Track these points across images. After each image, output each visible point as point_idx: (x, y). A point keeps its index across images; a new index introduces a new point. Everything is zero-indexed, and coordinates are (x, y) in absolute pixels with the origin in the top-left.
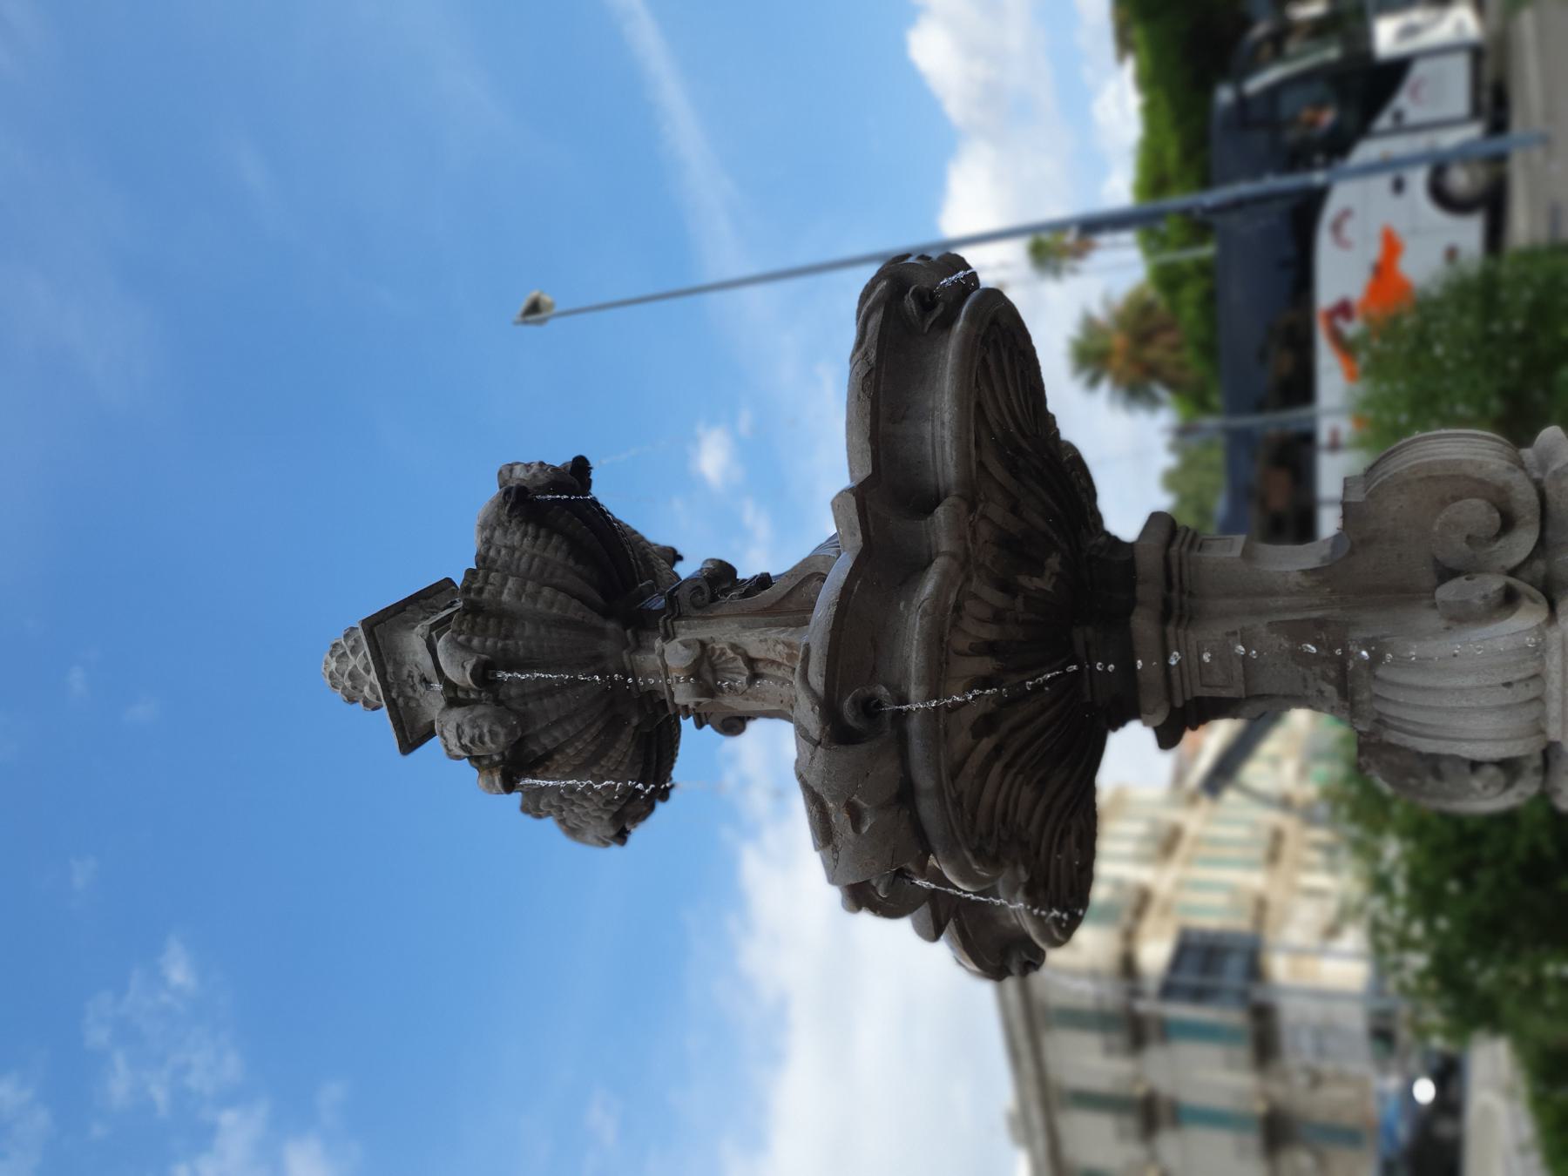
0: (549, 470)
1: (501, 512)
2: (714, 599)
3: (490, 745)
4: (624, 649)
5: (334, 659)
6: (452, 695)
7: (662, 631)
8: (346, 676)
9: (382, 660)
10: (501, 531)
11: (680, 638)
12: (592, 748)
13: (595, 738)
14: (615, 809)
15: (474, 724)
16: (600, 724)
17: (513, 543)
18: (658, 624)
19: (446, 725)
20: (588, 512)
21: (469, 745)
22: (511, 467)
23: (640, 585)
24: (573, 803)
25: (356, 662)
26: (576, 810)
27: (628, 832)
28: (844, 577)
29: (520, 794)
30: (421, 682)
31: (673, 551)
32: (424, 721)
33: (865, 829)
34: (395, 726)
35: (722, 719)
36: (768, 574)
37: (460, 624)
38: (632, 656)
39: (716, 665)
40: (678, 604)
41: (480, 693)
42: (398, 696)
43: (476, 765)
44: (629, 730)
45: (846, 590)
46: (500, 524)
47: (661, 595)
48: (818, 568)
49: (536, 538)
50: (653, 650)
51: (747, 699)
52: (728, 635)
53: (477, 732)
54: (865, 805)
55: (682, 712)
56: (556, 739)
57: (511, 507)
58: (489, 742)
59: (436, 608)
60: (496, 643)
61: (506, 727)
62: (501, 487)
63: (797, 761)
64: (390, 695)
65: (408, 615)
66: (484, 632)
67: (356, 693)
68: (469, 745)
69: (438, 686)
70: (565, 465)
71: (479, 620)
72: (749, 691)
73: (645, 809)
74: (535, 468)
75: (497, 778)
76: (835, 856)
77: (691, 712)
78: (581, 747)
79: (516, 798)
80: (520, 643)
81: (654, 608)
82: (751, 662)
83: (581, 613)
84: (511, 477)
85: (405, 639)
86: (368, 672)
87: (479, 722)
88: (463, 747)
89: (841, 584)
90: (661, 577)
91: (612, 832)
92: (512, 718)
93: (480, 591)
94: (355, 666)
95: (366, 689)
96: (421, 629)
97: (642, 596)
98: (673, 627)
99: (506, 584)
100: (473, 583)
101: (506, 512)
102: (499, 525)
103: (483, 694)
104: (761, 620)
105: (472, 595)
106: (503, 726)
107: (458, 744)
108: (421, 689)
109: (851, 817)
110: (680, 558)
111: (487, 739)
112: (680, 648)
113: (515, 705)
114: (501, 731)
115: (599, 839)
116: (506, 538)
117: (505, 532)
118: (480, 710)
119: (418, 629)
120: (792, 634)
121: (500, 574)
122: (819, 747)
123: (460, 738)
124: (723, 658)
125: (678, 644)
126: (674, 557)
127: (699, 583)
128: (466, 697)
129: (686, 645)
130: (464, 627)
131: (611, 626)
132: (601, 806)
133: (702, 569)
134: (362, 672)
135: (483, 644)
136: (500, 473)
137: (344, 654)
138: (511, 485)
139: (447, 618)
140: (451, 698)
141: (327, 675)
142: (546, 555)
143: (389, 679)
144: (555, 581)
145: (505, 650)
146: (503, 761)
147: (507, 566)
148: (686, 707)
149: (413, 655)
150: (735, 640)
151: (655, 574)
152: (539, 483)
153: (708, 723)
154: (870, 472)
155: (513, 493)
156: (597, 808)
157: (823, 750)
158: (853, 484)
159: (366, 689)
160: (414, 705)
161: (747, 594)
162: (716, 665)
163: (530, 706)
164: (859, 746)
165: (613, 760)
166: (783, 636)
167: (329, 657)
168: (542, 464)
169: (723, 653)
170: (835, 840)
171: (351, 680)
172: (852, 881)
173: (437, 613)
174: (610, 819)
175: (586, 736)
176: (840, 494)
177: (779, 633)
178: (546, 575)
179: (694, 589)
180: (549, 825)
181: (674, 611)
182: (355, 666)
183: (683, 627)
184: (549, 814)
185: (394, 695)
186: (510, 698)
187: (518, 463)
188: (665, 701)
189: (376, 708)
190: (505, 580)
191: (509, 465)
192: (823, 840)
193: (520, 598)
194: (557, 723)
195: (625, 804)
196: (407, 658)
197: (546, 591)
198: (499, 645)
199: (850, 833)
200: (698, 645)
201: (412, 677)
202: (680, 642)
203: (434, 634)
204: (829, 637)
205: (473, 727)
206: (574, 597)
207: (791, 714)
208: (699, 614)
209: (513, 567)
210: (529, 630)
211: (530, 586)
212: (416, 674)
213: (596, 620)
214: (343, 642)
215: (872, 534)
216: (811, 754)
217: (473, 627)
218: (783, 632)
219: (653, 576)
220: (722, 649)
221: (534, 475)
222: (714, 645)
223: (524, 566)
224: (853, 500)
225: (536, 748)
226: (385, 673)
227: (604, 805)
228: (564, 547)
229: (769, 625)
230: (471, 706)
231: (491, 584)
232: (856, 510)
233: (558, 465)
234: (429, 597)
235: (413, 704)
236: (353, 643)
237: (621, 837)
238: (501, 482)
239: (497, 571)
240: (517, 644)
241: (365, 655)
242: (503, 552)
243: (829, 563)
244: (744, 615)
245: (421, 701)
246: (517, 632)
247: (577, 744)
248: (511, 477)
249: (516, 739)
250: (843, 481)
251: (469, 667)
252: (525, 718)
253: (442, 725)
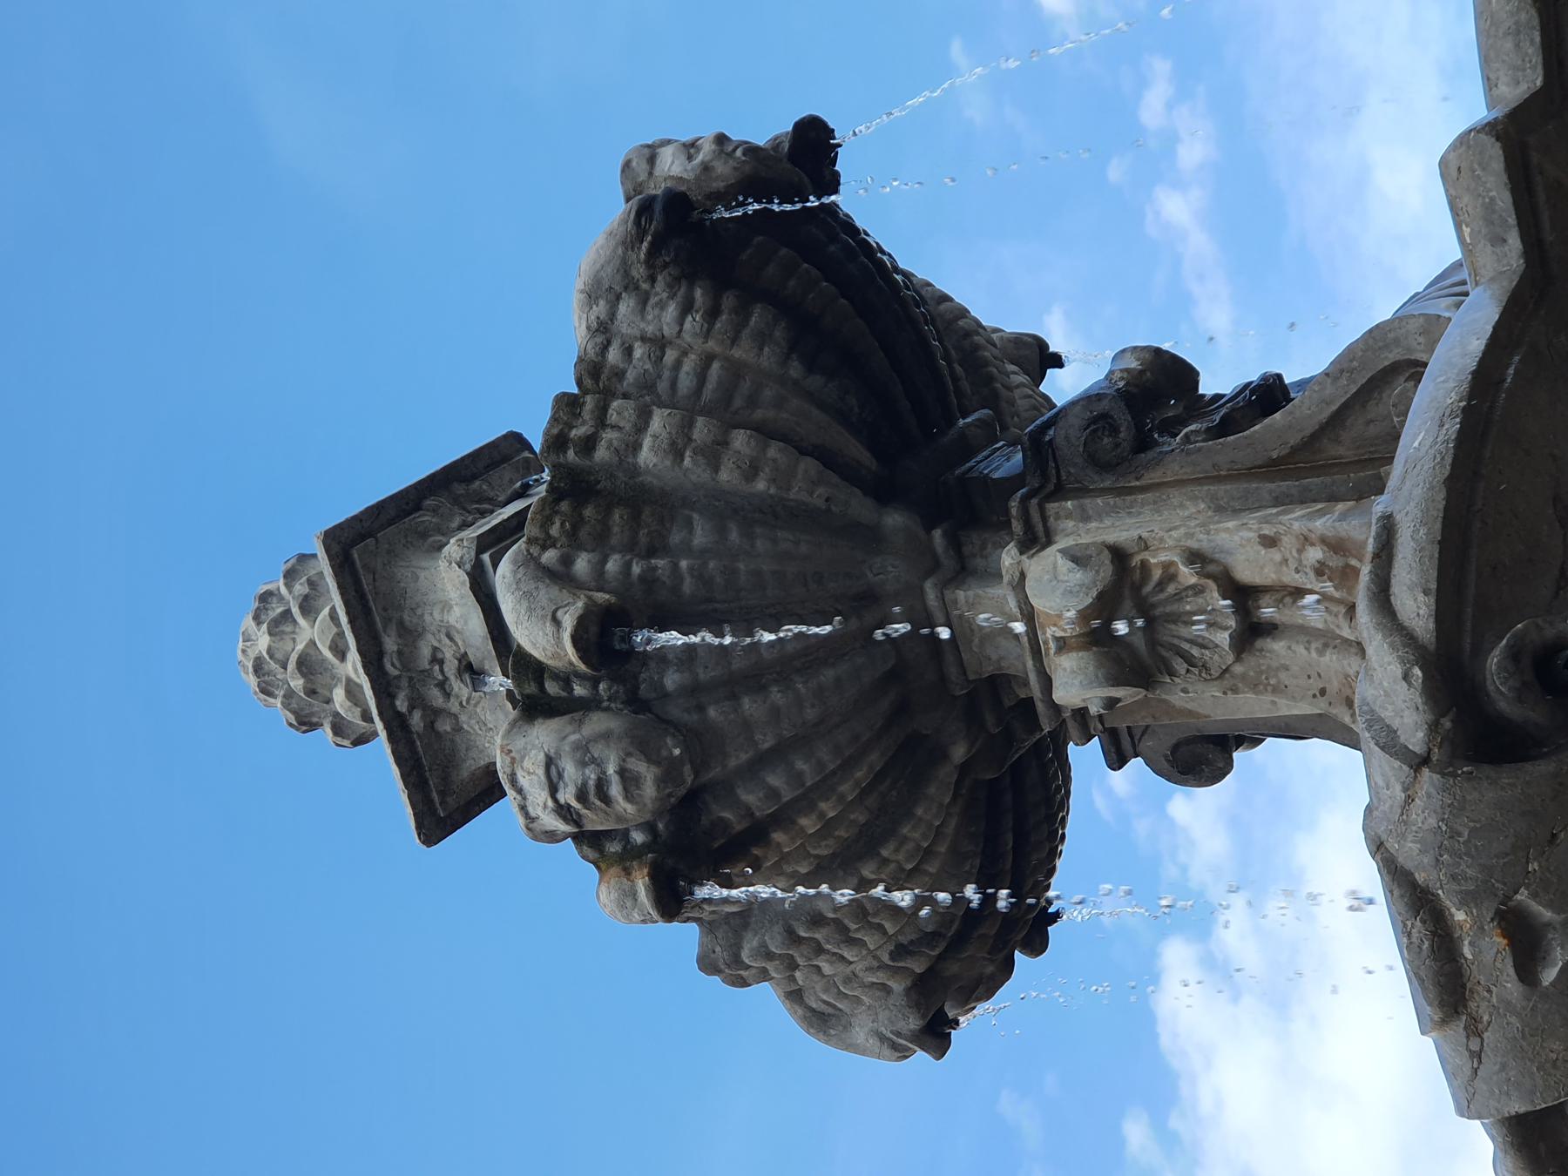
0: (739, 153)
1: (632, 256)
2: (1143, 443)
3: (622, 805)
4: (929, 573)
5: (264, 627)
6: (531, 689)
7: (1017, 526)
8: (292, 665)
9: (371, 625)
10: (632, 303)
11: (1062, 543)
12: (860, 817)
13: (864, 793)
14: (918, 966)
15: (584, 754)
16: (875, 759)
17: (661, 330)
18: (1007, 512)
19: (523, 758)
20: (832, 248)
21: (574, 804)
22: (651, 154)
23: (961, 422)
24: (819, 950)
25: (312, 633)
26: (827, 969)
27: (955, 1023)
28: (1477, 345)
29: (693, 928)
30: (460, 673)
31: (1041, 345)
32: (470, 765)
33: (1549, 975)
34: (405, 777)
35: (1174, 741)
36: (1279, 377)
37: (546, 523)
38: (948, 594)
39: (1153, 606)
40: (1055, 461)
41: (595, 683)
42: (412, 708)
43: (592, 854)
44: (946, 773)
45: (1485, 378)
46: (630, 285)
47: (1013, 444)
48: (1409, 350)
49: (712, 314)
50: (998, 576)
51: (1235, 690)
52: (1182, 531)
53: (591, 775)
54: (1547, 914)
55: (1073, 729)
56: (773, 794)
57: (652, 244)
58: (620, 800)
59: (490, 500)
60: (627, 566)
61: (658, 763)
62: (628, 200)
63: (1369, 810)
64: (393, 705)
65: (426, 518)
66: (601, 543)
67: (317, 705)
68: (574, 804)
69: (498, 682)
70: (776, 143)
71: (588, 512)
72: (1238, 669)
73: (990, 969)
74: (707, 150)
75: (641, 884)
76: (1475, 1045)
77: (1095, 725)
78: (831, 814)
79: (686, 936)
80: (684, 564)
81: (996, 475)
82: (1243, 595)
83: (820, 490)
84: (651, 174)
85: (422, 575)
86: (341, 654)
87: (597, 750)
88: (563, 811)
89: (1472, 364)
90: (1012, 403)
91: (913, 1023)
92: (669, 741)
93: (589, 444)
94: (312, 643)
95: (339, 695)
96: (457, 547)
97: (967, 448)
98: (1044, 519)
99: (647, 424)
100: (571, 427)
101: (642, 256)
102: (626, 288)
103: (602, 686)
104: (1268, 488)
105: (571, 454)
106: (649, 760)
107: (550, 803)
108: (461, 689)
109: (1512, 944)
110: (1057, 361)
111: (615, 790)
112: (1064, 564)
113: (675, 711)
114: (648, 774)
115: (882, 1038)
116: (643, 318)
117: (643, 301)
118: (597, 723)
119: (452, 549)
120: (1343, 517)
121: (631, 404)
122: (1426, 771)
123: (553, 790)
124: (1171, 589)
125: (1059, 556)
126: (1044, 359)
127: (1104, 405)
128: (564, 694)
129: (1078, 558)
130: (555, 531)
131: (894, 520)
132: (886, 958)
133: (1111, 372)
134: (327, 654)
135: (599, 569)
136: (627, 165)
137: (287, 615)
138: (654, 192)
139: (514, 522)
140: (528, 697)
141: (250, 665)
142: (737, 353)
143: (388, 667)
144: (759, 414)
145: (649, 580)
146: (654, 843)
147: (647, 386)
148: (1081, 714)
149: (442, 611)
150: (1201, 542)
151: (995, 395)
152: (719, 185)
153: (1136, 756)
154: (1539, 83)
155: (658, 207)
156: (875, 964)
157: (1436, 777)
158: (1497, 113)
159: (339, 695)
160: (448, 728)
161: (1225, 428)
162: (1153, 606)
163: (712, 712)
164: (1528, 766)
165: (910, 846)
166: (1321, 525)
167: (253, 624)
168: (721, 139)
169: (1169, 576)
170: (1472, 1005)
171: (303, 675)
172: (1518, 1107)
173: (492, 512)
174: (908, 991)
175: (844, 788)
176: (1463, 140)
177: (1311, 516)
178: (738, 402)
179: (1094, 420)
180: (765, 997)
181: (1045, 476)
182: (312, 643)
183: (1069, 516)
184: (764, 976)
185: (401, 704)
186: (665, 695)
187: (667, 142)
188: (1030, 701)
189: (360, 740)
190: (644, 416)
191: (649, 146)
192: (1442, 1005)
193: (678, 455)
194: (762, 761)
195: (940, 957)
196: (427, 618)
197: (740, 440)
198: (636, 569)
199: (1511, 986)
200: (1106, 557)
201: (441, 662)
202: (1060, 551)
203: (486, 557)
204: (1441, 496)
205: (582, 764)
206: (803, 452)
207: (1347, 720)
208: (1107, 484)
209: (662, 387)
210: (701, 536)
211: (702, 430)
212: (449, 654)
213: (860, 507)
214: (283, 590)
215: (1549, 237)
216: (1405, 790)
217: (575, 528)
218: (1321, 513)
219: (992, 400)
220: (1167, 566)
221: (706, 168)
222: (1145, 555)
223: (686, 382)
224: (1495, 151)
225: (727, 815)
226: (381, 654)
227: (893, 956)
228: (779, 333)
229: (1282, 501)
230: (577, 715)
231: (613, 427)
232: (1505, 178)
233: (761, 140)
234: (474, 477)
235: (444, 726)
236: (306, 590)
237: (936, 1035)
238: (630, 187)
239: (625, 396)
240: (675, 566)
241: (333, 616)
242: (638, 352)
243: (1433, 327)
244: (1218, 479)
245: (463, 718)
246: (676, 538)
247: (823, 806)
248: (651, 174)
249: (682, 791)
250: (1473, 108)
251: (568, 621)
252: (702, 744)
253: (513, 760)
